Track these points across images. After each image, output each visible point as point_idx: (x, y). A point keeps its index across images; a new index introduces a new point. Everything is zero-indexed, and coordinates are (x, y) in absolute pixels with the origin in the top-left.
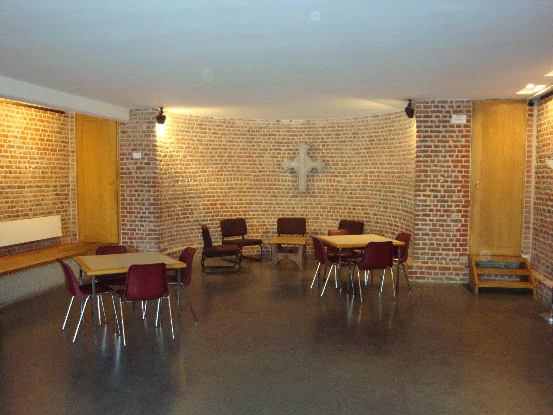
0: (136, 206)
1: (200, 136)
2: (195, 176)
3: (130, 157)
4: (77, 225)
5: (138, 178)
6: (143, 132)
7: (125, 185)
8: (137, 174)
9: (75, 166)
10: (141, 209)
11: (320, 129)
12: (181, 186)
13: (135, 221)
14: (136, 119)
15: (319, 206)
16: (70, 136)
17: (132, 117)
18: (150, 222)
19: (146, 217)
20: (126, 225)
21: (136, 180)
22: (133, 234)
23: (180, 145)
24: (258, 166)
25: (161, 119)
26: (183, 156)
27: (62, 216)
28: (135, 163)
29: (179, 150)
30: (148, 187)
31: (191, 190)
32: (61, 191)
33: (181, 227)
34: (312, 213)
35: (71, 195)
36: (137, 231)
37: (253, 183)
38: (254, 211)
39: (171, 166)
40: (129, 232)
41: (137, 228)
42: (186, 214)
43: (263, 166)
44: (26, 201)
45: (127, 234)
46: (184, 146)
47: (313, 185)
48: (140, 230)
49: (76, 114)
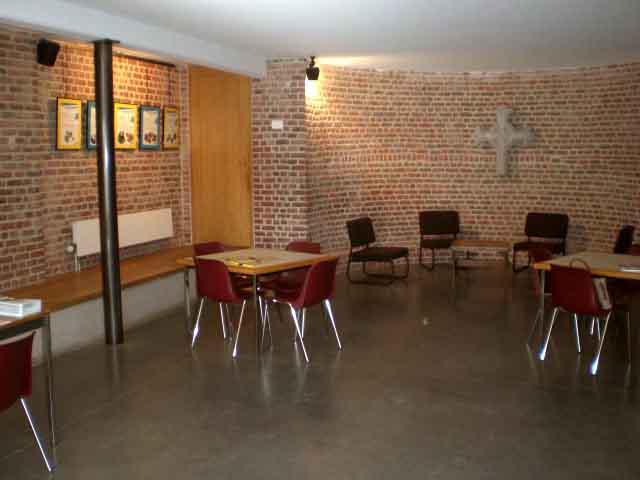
1: (358, 97)
3: (267, 126)
4: (191, 221)
5: (279, 156)
7: (260, 166)
10: (283, 199)
11: (528, 85)
12: (333, 167)
15: (525, 195)
16: (181, 98)
18: (295, 217)
19: (289, 211)
21: (275, 159)
24: (437, 138)
25: (313, 74)
26: (337, 125)
27: (173, 208)
28: (275, 136)
29: (332, 116)
30: (294, 168)
33: (333, 224)
34: (515, 205)
36: (277, 231)
37: (430, 163)
38: (432, 202)
39: (321, 140)
40: (266, 232)
41: (276, 226)
42: (339, 206)
43: (444, 138)
45: (263, 234)
46: (338, 111)
47: (516, 166)
48: (280, 228)
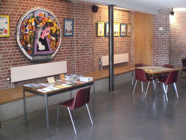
0: (160, 50)
2: (184, 38)
5: (161, 38)
6: (164, 19)
7: (155, 41)
8: (161, 37)
9: (134, 33)
12: (178, 42)
13: (159, 57)
14: (161, 13)
17: (11, 29)
18: (165, 57)
19: (164, 55)
20: (155, 58)
22: (158, 62)
23: (178, 24)
25: (172, 13)
26: (179, 29)
28: (160, 32)
30: (166, 42)
31: (182, 44)
32: (129, 43)
35: (132, 45)
36: (160, 61)
39: (174, 33)
40: (156, 61)
41: (160, 60)
44: (117, 48)
48: (161, 60)
49: (135, 12)
